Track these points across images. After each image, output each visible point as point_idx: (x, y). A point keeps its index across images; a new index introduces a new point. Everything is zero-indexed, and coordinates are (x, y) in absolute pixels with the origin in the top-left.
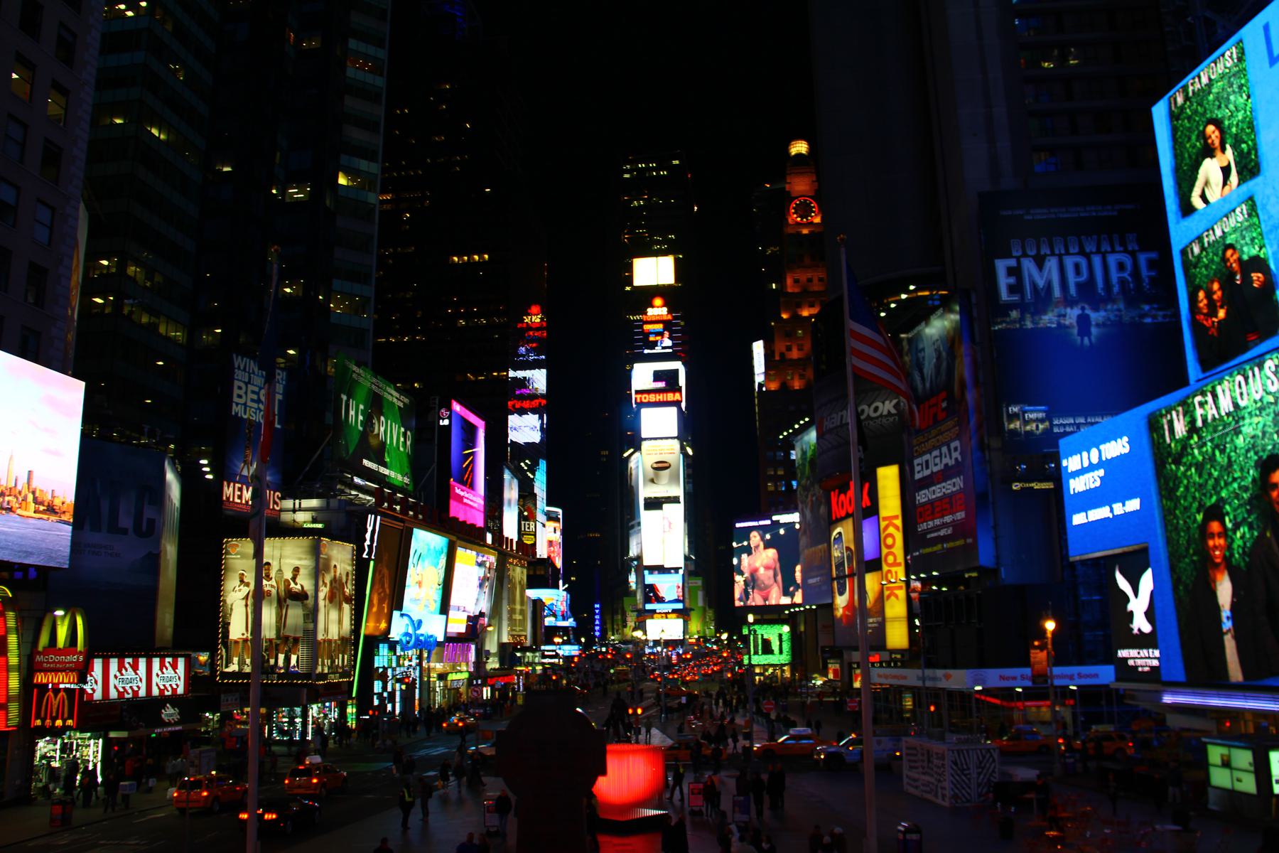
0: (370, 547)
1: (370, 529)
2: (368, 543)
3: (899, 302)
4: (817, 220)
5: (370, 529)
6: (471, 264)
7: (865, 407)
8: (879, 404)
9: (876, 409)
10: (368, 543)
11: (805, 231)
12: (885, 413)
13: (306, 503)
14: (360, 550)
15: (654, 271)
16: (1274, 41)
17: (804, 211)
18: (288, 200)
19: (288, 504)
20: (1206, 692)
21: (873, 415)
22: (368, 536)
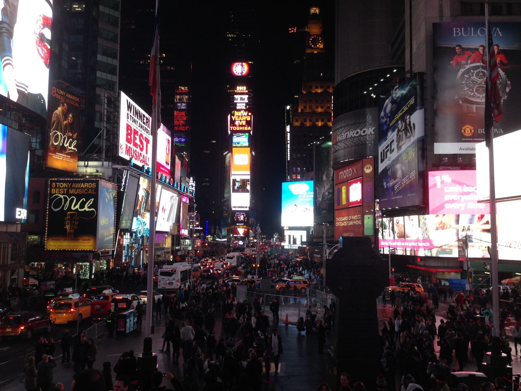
0: (125, 186)
1: (124, 177)
2: (123, 184)
3: (378, 82)
4: (322, 46)
5: (124, 177)
6: (48, 230)
7: (359, 130)
8: (366, 130)
9: (364, 132)
10: (123, 184)
11: (315, 52)
12: (369, 133)
13: (91, 163)
14: (119, 187)
15: (239, 69)
16: (413, 25)
17: (315, 42)
18: (73, 11)
19: (82, 163)
20: (6, 145)
21: (362, 134)
22: (123, 180)
